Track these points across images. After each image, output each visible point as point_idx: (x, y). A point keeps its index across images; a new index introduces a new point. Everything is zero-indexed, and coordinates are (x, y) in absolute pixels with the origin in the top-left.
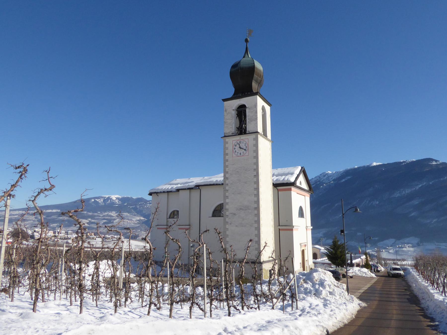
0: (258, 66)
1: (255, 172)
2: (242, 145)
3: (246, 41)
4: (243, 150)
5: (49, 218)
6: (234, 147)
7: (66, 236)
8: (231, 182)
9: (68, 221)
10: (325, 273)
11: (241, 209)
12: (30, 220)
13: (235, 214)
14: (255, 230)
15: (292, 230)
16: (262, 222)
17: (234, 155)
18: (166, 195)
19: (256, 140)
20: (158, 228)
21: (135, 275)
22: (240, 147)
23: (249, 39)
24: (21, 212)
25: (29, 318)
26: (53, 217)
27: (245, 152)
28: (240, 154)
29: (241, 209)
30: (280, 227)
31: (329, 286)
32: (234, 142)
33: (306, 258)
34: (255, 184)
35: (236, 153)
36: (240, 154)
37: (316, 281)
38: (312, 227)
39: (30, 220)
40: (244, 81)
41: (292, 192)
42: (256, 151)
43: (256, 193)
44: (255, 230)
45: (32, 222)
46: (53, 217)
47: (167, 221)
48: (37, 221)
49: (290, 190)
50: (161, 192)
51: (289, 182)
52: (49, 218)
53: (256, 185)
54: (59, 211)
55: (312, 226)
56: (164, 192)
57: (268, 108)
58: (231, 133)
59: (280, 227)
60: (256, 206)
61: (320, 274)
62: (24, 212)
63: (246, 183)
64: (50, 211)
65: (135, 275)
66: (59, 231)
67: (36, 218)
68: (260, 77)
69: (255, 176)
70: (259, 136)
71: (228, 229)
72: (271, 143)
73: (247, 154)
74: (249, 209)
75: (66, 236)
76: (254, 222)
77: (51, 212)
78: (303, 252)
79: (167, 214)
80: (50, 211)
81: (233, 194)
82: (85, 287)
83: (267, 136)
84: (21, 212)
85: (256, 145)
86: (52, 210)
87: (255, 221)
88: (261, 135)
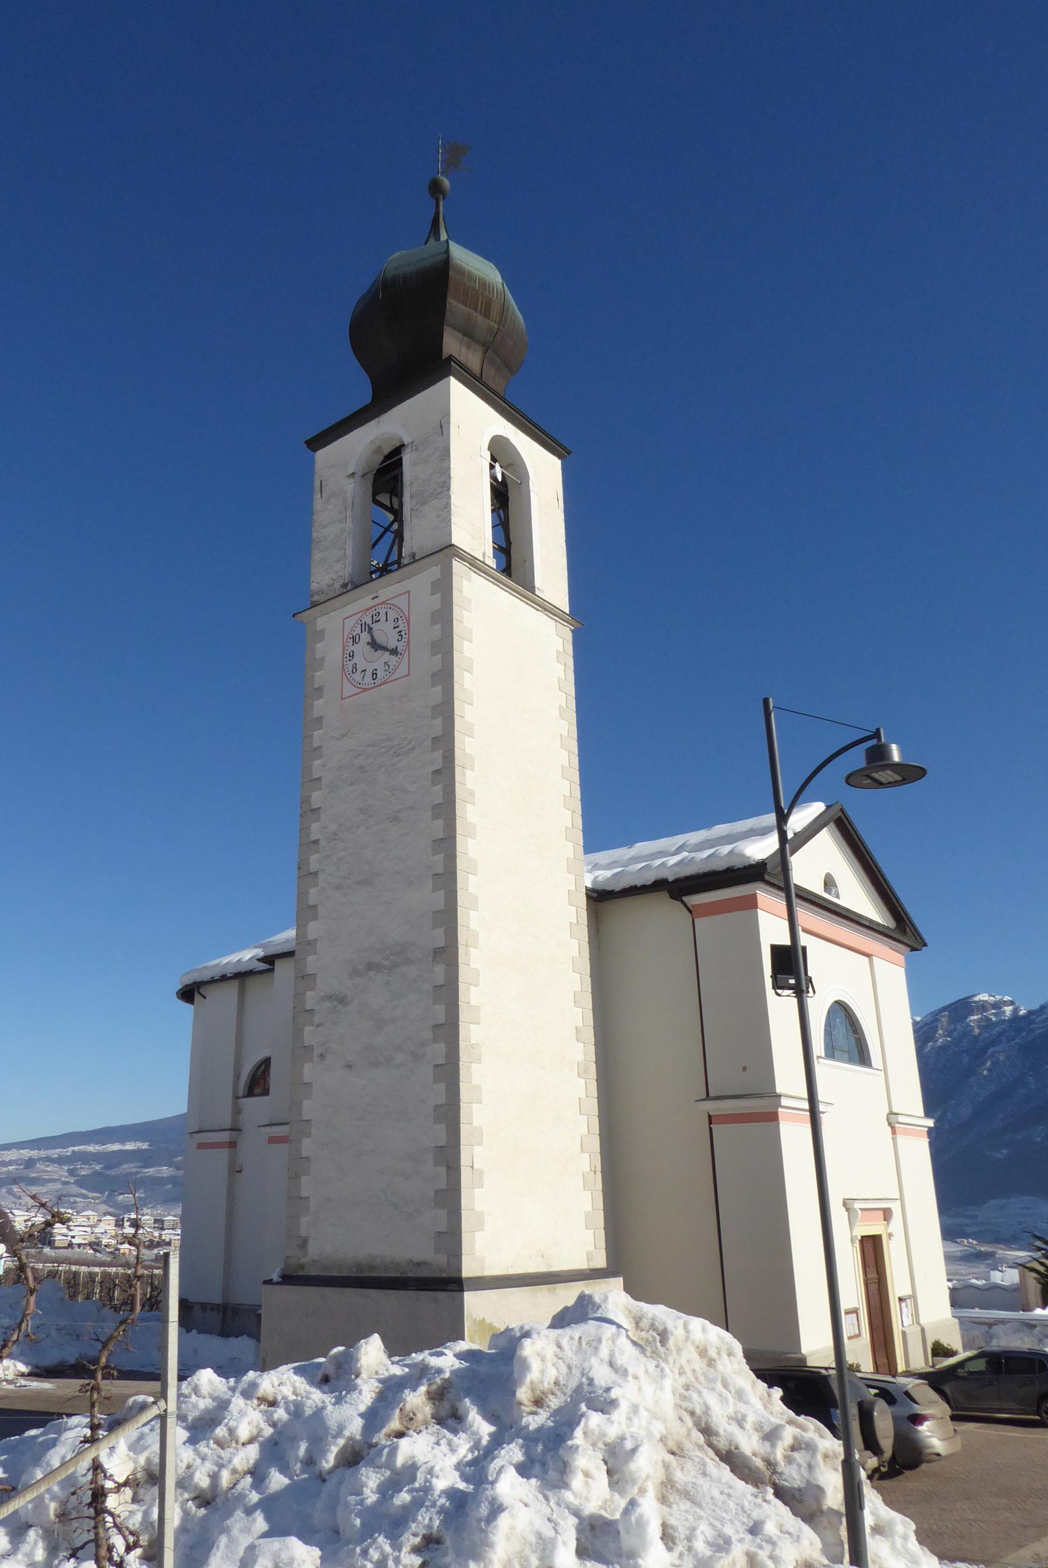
0: (469, 262)
1: (438, 754)
2: (385, 632)
3: (435, 189)
4: (387, 656)
5: (113, 1172)
6: (351, 648)
7: (156, 1234)
8: (333, 827)
9: (172, 1180)
10: (664, 1335)
11: (371, 966)
12: (55, 1181)
13: (342, 1000)
14: (436, 1080)
15: (773, 1117)
16: (470, 1033)
17: (349, 690)
18: (233, 988)
19: (444, 587)
20: (201, 1146)
21: (23, 1368)
22: (375, 645)
23: (446, 182)
24: (26, 1153)
25: (503, 1511)
26: (127, 1168)
27: (393, 660)
28: (374, 674)
29: (371, 966)
30: (713, 1107)
31: (616, 1460)
32: (349, 624)
33: (897, 1285)
34: (435, 817)
35: (358, 676)
36: (374, 674)
37: (538, 1402)
38: (930, 1123)
39: (55, 1181)
40: (404, 340)
41: (762, 916)
42: (443, 647)
43: (439, 870)
44: (436, 1080)
45: (58, 1186)
46: (127, 1168)
47: (237, 1111)
48: (76, 1182)
49: (751, 903)
50: (212, 981)
51: (738, 863)
52: (113, 1172)
53: (439, 823)
54: (145, 1146)
55: (928, 1114)
56: (224, 978)
57: (544, 472)
58: (337, 586)
59: (713, 1107)
60: (438, 938)
61: (595, 1343)
62: (34, 1153)
63: (395, 819)
64: (116, 1147)
65: (23, 1368)
66: (133, 1216)
67: (71, 1173)
68: (486, 315)
69: (437, 772)
70: (457, 566)
71: (309, 1085)
72: (567, 632)
73: (403, 670)
74: (409, 962)
75: (156, 1234)
76: (428, 1034)
77: (120, 1151)
78: (872, 1250)
79: (237, 1077)
80: (116, 1147)
81: (339, 887)
82: (471, 1426)
83: (531, 588)
84: (26, 1153)
85: (443, 617)
86: (123, 1142)
87: (436, 1026)
88: (473, 563)
